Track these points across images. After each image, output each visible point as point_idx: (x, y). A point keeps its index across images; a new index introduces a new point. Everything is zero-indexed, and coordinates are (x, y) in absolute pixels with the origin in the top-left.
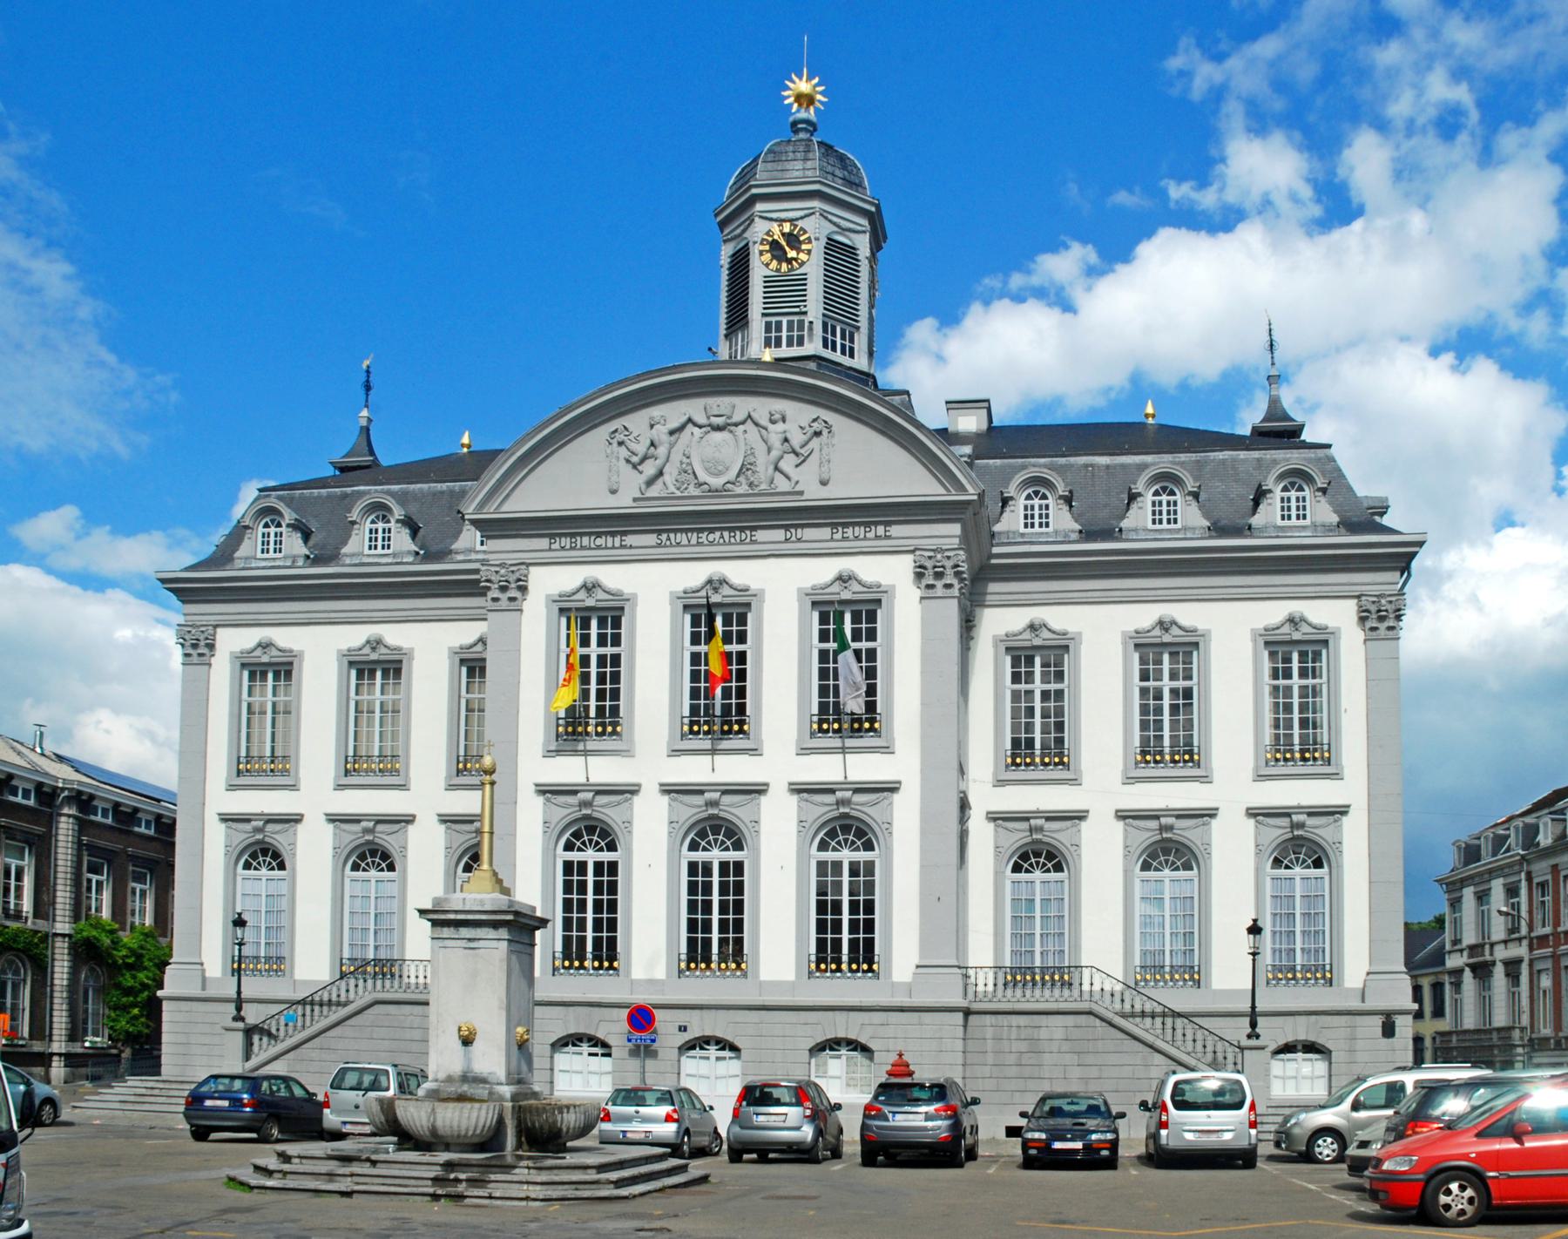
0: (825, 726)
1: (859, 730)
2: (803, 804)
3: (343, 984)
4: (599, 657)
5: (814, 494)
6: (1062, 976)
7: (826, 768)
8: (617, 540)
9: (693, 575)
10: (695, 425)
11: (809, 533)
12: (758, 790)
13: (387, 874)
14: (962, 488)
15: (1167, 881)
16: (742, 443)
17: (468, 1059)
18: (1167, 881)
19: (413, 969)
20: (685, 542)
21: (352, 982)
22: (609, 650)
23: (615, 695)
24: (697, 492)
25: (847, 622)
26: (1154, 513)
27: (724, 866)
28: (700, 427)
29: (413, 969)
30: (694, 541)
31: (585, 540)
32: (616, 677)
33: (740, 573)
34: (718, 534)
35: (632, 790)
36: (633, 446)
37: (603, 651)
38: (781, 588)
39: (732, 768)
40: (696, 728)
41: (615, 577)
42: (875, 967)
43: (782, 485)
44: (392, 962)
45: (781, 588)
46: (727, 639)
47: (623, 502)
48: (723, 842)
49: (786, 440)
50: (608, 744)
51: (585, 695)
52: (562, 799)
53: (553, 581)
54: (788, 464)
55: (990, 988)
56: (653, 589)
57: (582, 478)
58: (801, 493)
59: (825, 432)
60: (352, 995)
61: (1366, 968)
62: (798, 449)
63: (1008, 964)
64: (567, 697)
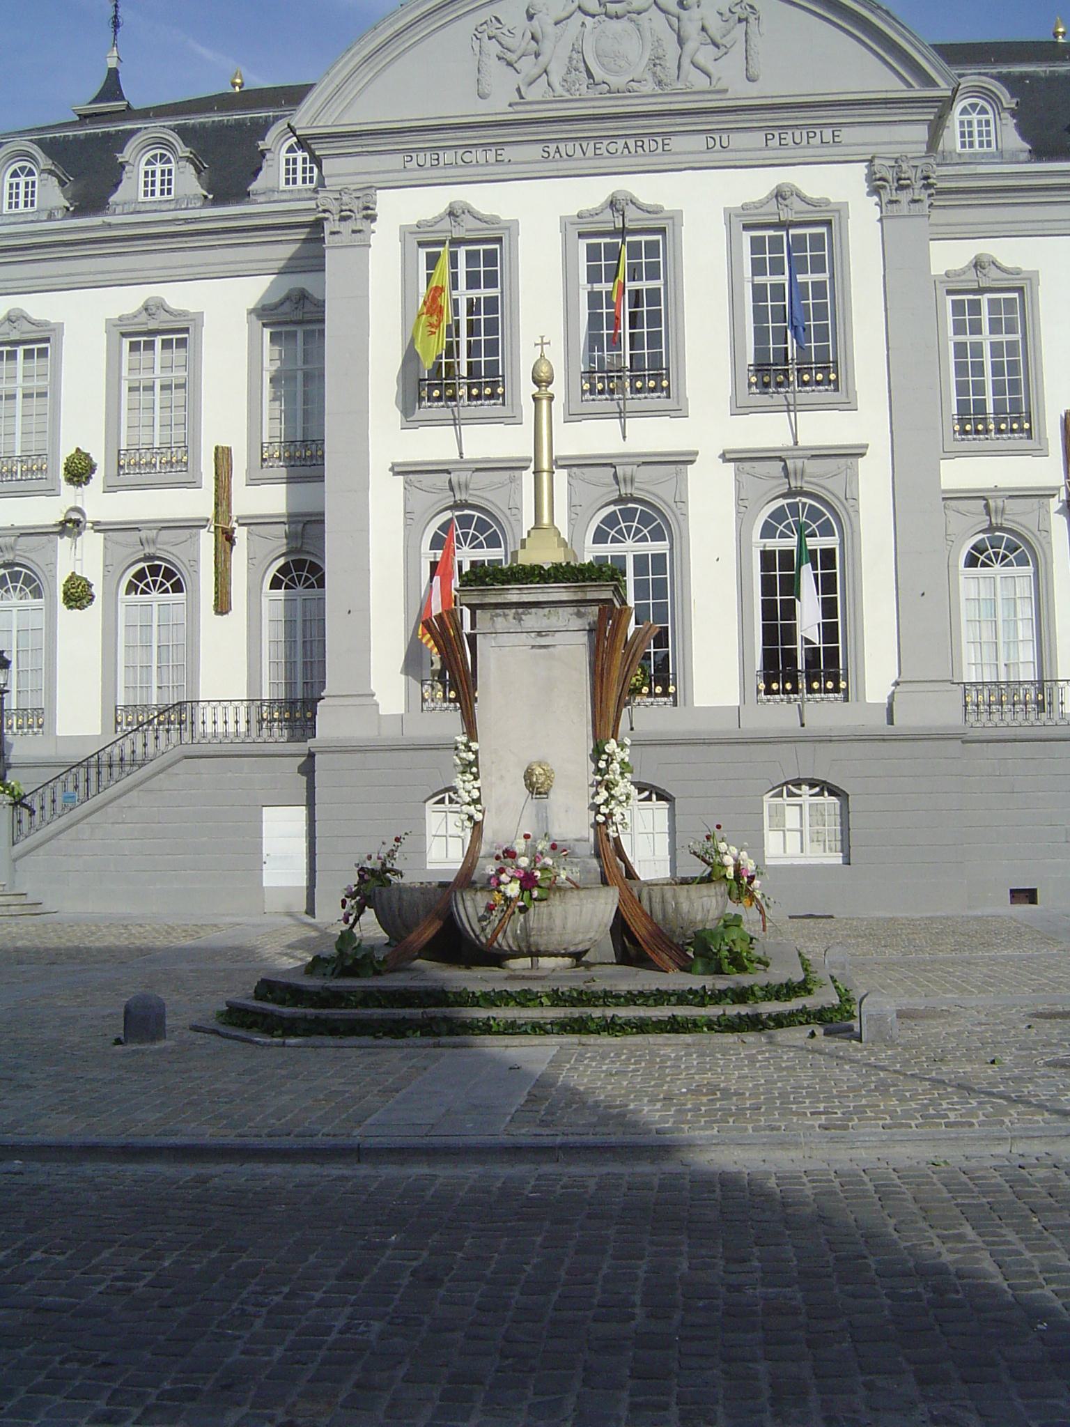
0: (639, 384)
1: (478, 397)
2: (744, 478)
3: (140, 736)
4: (470, 301)
5: (741, 92)
6: (178, 713)
7: (768, 430)
8: (491, 156)
9: (589, 194)
10: (586, 13)
11: (738, 140)
12: (684, 460)
13: (31, 601)
14: (929, 82)
15: (155, 605)
16: (647, 34)
17: (543, 818)
18: (155, 605)
19: (209, 711)
20: (579, 153)
21: (151, 735)
22: (483, 293)
23: (492, 348)
24: (592, 94)
25: (791, 251)
26: (287, 171)
27: (640, 561)
28: (593, 16)
29: (209, 711)
30: (590, 153)
31: (449, 156)
32: (492, 327)
33: (650, 190)
34: (621, 142)
35: (684, 460)
36: (507, 41)
37: (474, 294)
38: (703, 206)
39: (650, 434)
40: (639, 384)
41: (490, 200)
42: (671, 689)
43: (701, 82)
44: (38, 712)
45: (703, 206)
46: (634, 274)
47: (498, 106)
48: (475, 538)
49: (703, 29)
50: (487, 408)
51: (451, 350)
52: (760, 467)
53: (404, 208)
54: (705, 56)
55: (243, 727)
56: (540, 215)
57: (434, 78)
58: (726, 91)
59: (752, 19)
60: (151, 749)
61: (895, 677)
62: (718, 40)
63: (300, 696)
64: (431, 349)
